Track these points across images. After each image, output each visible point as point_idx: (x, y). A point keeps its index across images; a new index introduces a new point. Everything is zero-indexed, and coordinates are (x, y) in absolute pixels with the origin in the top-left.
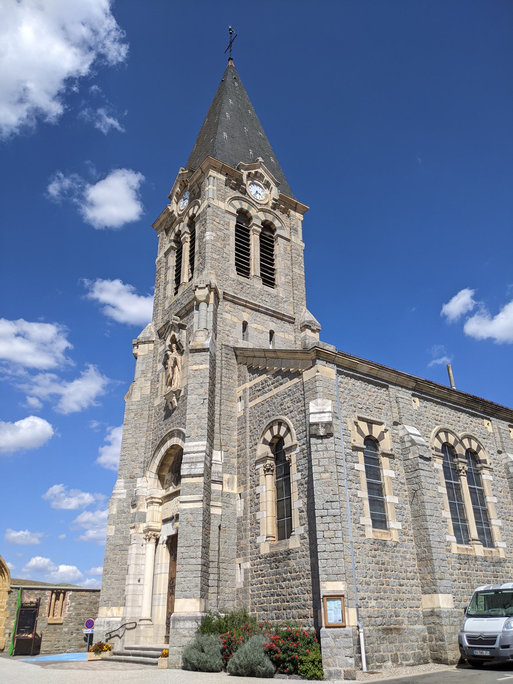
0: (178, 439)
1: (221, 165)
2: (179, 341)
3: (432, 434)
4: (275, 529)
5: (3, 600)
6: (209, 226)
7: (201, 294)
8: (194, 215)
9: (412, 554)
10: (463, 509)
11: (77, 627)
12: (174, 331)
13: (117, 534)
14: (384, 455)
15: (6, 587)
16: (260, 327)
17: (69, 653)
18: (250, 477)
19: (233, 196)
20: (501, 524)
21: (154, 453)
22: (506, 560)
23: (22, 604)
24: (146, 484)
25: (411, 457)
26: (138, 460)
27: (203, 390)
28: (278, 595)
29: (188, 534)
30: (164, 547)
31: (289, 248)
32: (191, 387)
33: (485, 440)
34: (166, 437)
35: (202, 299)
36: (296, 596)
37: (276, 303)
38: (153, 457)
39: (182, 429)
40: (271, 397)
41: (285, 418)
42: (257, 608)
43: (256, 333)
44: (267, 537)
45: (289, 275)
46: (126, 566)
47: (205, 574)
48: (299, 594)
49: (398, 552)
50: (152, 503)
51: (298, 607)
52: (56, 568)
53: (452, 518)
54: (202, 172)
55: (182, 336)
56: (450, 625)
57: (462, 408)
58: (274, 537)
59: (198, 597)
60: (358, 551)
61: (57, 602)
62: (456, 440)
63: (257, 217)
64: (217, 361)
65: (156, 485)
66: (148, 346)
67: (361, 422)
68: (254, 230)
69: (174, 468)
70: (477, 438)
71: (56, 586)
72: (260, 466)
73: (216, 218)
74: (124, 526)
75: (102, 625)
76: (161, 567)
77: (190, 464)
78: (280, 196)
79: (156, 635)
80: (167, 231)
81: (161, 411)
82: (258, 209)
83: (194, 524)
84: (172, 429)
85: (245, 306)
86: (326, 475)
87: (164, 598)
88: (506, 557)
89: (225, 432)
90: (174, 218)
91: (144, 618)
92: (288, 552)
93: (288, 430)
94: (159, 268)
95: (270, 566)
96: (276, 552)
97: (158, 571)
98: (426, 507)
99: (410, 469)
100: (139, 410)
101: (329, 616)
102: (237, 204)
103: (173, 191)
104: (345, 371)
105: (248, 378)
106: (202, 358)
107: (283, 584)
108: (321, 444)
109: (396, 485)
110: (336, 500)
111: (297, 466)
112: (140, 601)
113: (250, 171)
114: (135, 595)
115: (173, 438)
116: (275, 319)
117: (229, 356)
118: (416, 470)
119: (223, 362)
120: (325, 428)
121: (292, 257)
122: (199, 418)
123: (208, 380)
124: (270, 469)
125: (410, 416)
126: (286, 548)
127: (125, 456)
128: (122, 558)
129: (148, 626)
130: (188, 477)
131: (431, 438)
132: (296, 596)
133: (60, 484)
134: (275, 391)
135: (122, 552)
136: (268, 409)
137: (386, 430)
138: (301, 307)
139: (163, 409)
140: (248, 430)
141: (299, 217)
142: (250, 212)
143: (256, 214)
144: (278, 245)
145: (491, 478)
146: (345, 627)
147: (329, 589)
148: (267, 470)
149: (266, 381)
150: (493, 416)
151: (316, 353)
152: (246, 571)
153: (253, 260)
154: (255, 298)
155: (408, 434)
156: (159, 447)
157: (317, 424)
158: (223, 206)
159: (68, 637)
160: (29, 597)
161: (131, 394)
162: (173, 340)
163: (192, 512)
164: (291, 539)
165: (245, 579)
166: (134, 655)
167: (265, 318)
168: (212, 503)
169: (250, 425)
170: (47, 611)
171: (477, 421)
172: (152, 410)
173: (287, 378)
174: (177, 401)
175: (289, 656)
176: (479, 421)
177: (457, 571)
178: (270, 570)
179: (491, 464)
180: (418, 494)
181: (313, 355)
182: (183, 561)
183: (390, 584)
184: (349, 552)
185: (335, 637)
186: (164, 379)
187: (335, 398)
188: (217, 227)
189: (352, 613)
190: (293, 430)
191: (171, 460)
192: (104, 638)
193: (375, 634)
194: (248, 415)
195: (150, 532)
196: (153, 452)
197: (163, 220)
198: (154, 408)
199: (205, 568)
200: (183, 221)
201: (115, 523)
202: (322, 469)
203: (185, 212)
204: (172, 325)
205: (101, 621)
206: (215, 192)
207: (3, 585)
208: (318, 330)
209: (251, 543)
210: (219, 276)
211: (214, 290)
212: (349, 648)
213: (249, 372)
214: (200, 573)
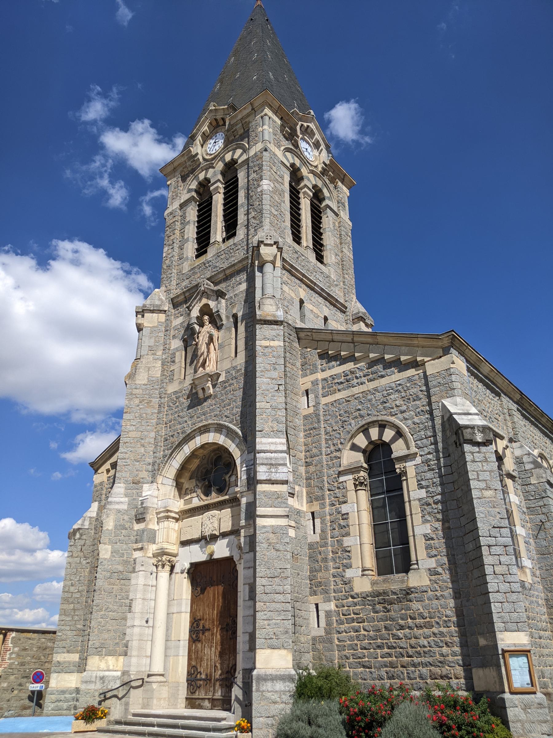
0: (218, 435)
1: (278, 105)
2: (218, 311)
4: (374, 560)
11: (19, 681)
13: (114, 556)
16: (315, 310)
17: (8, 717)
18: (328, 492)
25: (533, 481)
26: (144, 461)
27: (277, 374)
29: (271, 561)
30: (185, 578)
32: (260, 367)
35: (269, 259)
36: (426, 649)
40: (362, 392)
42: (350, 664)
46: (127, 601)
48: (430, 647)
50: (168, 517)
51: (425, 665)
54: (253, 109)
58: (373, 571)
59: (289, 647)
65: (172, 495)
66: (158, 316)
68: (305, 193)
69: (199, 474)
74: (125, 546)
75: (92, 682)
77: (269, 467)
78: (331, 161)
79: (173, 696)
80: (184, 179)
82: (310, 170)
83: (278, 546)
84: (205, 423)
85: (301, 280)
87: (184, 647)
90: (197, 163)
91: (156, 673)
92: (408, 592)
93: (399, 434)
94: (171, 221)
95: (373, 609)
96: (383, 590)
99: (532, 496)
100: (146, 396)
103: (199, 130)
104: (471, 368)
105: (320, 367)
106: (274, 333)
107: (400, 633)
108: (479, 452)
110: (505, 526)
111: (418, 481)
114: (142, 640)
115: (207, 434)
117: (291, 338)
120: (482, 432)
121: (340, 235)
122: (273, 408)
124: (363, 482)
126: (404, 586)
127: (126, 453)
128: (122, 589)
129: (162, 684)
130: (266, 484)
134: (371, 385)
135: (122, 581)
136: (360, 407)
137: (507, 447)
139: (186, 397)
140: (323, 432)
142: (302, 170)
143: (307, 174)
146: (534, 693)
147: (508, 642)
148: (358, 484)
149: (352, 372)
151: (452, 339)
152: (328, 614)
161: (135, 374)
167: (320, 301)
169: (326, 425)
172: (165, 397)
178: (372, 614)
180: (546, 526)
181: (446, 342)
192: (95, 699)
197: (179, 164)
198: (166, 396)
202: (483, 485)
203: (218, 156)
205: (91, 676)
212: (546, 722)
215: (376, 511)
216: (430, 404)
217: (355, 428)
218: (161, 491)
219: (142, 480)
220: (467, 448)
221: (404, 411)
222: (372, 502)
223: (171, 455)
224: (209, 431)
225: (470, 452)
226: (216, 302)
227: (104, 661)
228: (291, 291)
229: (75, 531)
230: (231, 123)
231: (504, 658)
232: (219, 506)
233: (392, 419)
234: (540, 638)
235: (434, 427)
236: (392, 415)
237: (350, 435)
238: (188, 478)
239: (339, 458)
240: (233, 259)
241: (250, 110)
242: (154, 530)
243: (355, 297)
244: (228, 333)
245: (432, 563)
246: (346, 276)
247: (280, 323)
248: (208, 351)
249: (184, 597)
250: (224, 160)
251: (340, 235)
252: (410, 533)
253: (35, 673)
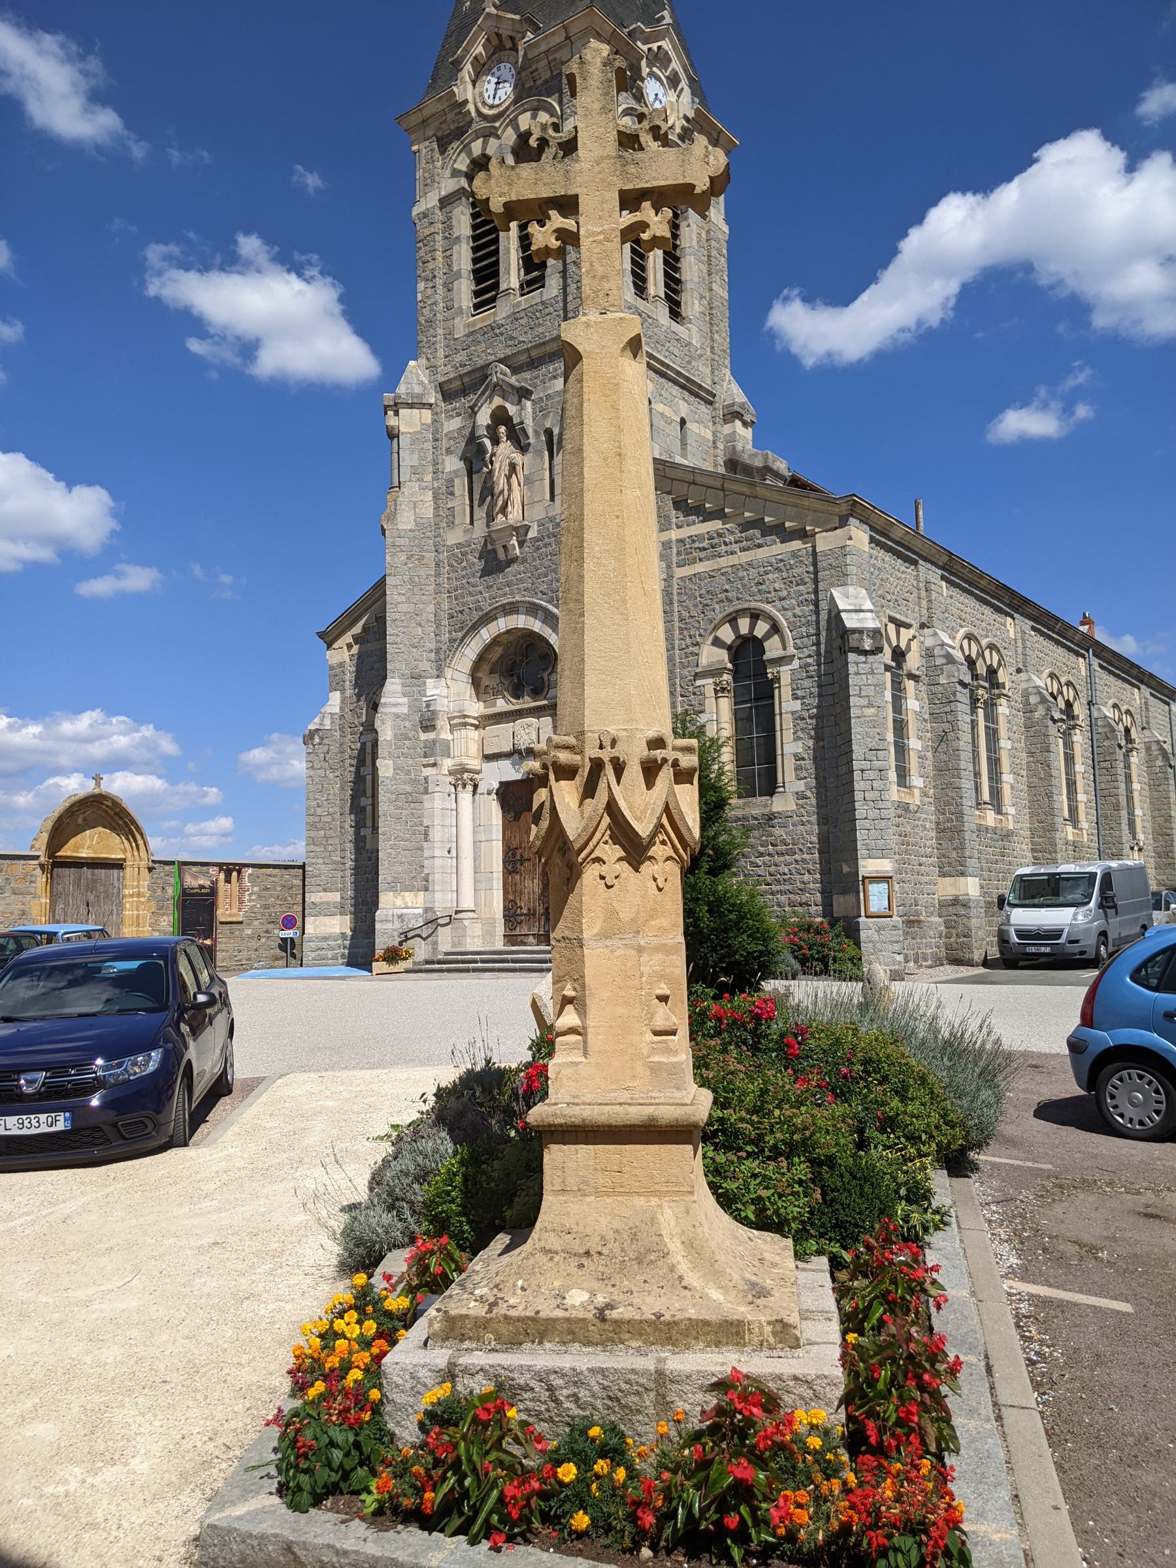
0: (532, 619)
1: (611, 30)
23: (184, 890)
46: (422, 828)
49: (919, 819)
50: (465, 725)
54: (568, 38)
74: (410, 762)
78: (697, 111)
79: (489, 934)
86: (870, 711)
90: (467, 119)
92: (771, 817)
93: (775, 629)
103: (466, 50)
105: (674, 520)
107: (759, 861)
108: (865, 663)
111: (793, 690)
115: (515, 616)
120: (872, 638)
121: (709, 256)
126: (767, 811)
134: (745, 557)
136: (727, 587)
137: (914, 637)
139: (477, 555)
140: (676, 619)
146: (891, 917)
148: (720, 690)
149: (720, 535)
150: (1016, 610)
156: (475, 628)
159: (254, 944)
166: (514, 961)
167: (674, 393)
175: (819, 952)
181: (844, 509)
185: (879, 930)
202: (864, 702)
215: (739, 723)
216: (816, 592)
217: (721, 616)
218: (452, 688)
220: (852, 657)
221: (784, 599)
222: (736, 713)
223: (462, 640)
224: (517, 612)
226: (518, 407)
229: (312, 734)
230: (530, 56)
231: (863, 884)
232: (537, 712)
233: (768, 608)
234: (920, 865)
235: (818, 622)
236: (769, 603)
237: (712, 626)
238: (487, 672)
239: (697, 655)
240: (541, 330)
241: (563, 39)
243: (728, 372)
244: (538, 461)
245: (801, 786)
246: (716, 337)
248: (510, 490)
249: (494, 823)
250: (518, 125)
251: (709, 256)
252: (779, 752)
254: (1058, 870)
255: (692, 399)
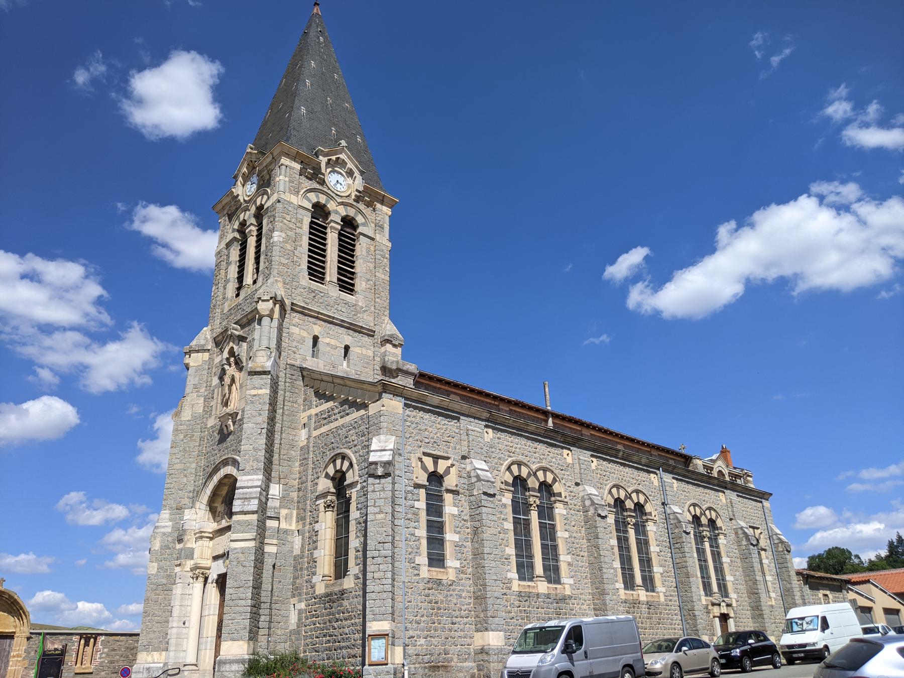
0: (233, 468)
1: (296, 152)
2: (238, 355)
3: (504, 468)
5: (21, 648)
6: (278, 225)
7: (264, 307)
8: (262, 206)
9: (468, 592)
10: (530, 545)
12: (233, 342)
13: (159, 572)
14: (448, 491)
15: (24, 633)
19: (308, 188)
20: (570, 560)
21: (206, 482)
22: (572, 597)
23: (44, 652)
24: (195, 516)
25: (475, 493)
28: (331, 636)
31: (372, 248)
33: (563, 472)
34: (219, 465)
36: (347, 636)
37: (353, 313)
38: (204, 486)
39: (237, 458)
41: (349, 452)
42: (309, 649)
43: (328, 348)
44: (323, 577)
45: (371, 280)
47: (255, 615)
49: (453, 590)
50: (202, 537)
52: (74, 606)
53: (516, 555)
54: (273, 158)
55: (242, 350)
56: (498, 662)
57: (540, 438)
58: (331, 577)
60: (410, 591)
61: (87, 648)
62: (529, 472)
63: (337, 212)
64: (280, 383)
65: (207, 518)
67: (427, 458)
68: (332, 227)
70: (554, 470)
71: (71, 630)
72: (321, 502)
73: (287, 216)
74: (168, 563)
76: (209, 609)
77: (243, 500)
78: (364, 187)
80: (230, 217)
81: (215, 433)
82: (338, 203)
86: (380, 516)
87: (212, 641)
88: (572, 594)
89: (285, 463)
90: (239, 203)
92: (343, 592)
93: (351, 465)
97: (206, 613)
98: (485, 545)
101: (372, 654)
102: (313, 197)
104: (413, 404)
105: (315, 403)
106: (262, 382)
108: (379, 484)
109: (458, 523)
111: (357, 504)
112: (185, 646)
113: (330, 157)
116: (351, 332)
117: (294, 377)
118: (479, 507)
119: (287, 384)
120: (383, 467)
122: (255, 449)
123: (267, 407)
125: (480, 450)
127: (171, 483)
128: (165, 598)
131: (502, 471)
132: (347, 636)
133: (82, 491)
134: (341, 422)
136: (333, 441)
137: (453, 465)
138: (383, 318)
139: (217, 432)
140: (310, 462)
141: (387, 210)
142: (328, 206)
143: (335, 208)
144: (360, 244)
145: (565, 512)
149: (333, 409)
153: (329, 262)
154: (329, 308)
155: (475, 469)
156: (211, 476)
157: (376, 463)
158: (295, 200)
160: (53, 643)
162: (232, 353)
163: (243, 551)
164: (346, 579)
165: (299, 620)
168: (266, 541)
170: (74, 659)
171: (556, 451)
173: (354, 409)
174: (234, 425)
176: (559, 451)
177: (516, 609)
179: (566, 497)
181: (380, 388)
182: (231, 603)
183: (442, 622)
184: (401, 592)
185: (378, 674)
186: (220, 397)
187: (400, 434)
188: (288, 226)
189: (399, 650)
190: (355, 466)
191: (224, 491)
193: (421, 671)
194: (311, 445)
195: (198, 570)
196: (204, 480)
199: (255, 609)
200: (249, 210)
201: (157, 560)
202: (377, 510)
203: (252, 200)
204: (231, 336)
206: (287, 183)
207: (20, 630)
208: (401, 345)
209: (307, 582)
210: (287, 284)
211: (279, 302)
213: (316, 397)
214: (249, 614)
219: (184, 506)
225: (372, 484)
227: (150, 656)
228: (302, 331)
238: (220, 503)
242: (192, 548)
247: (268, 373)
249: (213, 602)
253: (123, 669)
254: (546, 625)
255: (356, 334)
